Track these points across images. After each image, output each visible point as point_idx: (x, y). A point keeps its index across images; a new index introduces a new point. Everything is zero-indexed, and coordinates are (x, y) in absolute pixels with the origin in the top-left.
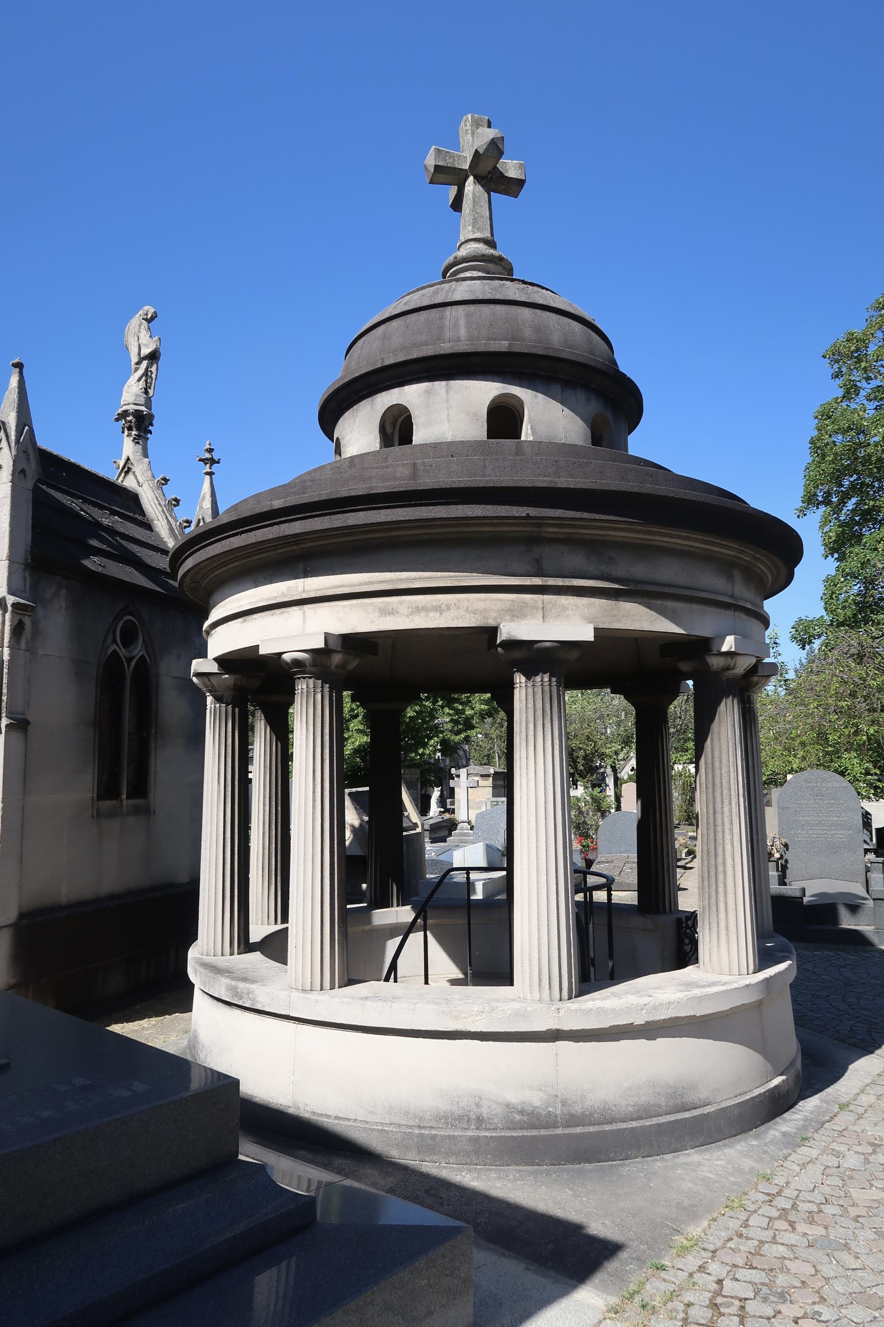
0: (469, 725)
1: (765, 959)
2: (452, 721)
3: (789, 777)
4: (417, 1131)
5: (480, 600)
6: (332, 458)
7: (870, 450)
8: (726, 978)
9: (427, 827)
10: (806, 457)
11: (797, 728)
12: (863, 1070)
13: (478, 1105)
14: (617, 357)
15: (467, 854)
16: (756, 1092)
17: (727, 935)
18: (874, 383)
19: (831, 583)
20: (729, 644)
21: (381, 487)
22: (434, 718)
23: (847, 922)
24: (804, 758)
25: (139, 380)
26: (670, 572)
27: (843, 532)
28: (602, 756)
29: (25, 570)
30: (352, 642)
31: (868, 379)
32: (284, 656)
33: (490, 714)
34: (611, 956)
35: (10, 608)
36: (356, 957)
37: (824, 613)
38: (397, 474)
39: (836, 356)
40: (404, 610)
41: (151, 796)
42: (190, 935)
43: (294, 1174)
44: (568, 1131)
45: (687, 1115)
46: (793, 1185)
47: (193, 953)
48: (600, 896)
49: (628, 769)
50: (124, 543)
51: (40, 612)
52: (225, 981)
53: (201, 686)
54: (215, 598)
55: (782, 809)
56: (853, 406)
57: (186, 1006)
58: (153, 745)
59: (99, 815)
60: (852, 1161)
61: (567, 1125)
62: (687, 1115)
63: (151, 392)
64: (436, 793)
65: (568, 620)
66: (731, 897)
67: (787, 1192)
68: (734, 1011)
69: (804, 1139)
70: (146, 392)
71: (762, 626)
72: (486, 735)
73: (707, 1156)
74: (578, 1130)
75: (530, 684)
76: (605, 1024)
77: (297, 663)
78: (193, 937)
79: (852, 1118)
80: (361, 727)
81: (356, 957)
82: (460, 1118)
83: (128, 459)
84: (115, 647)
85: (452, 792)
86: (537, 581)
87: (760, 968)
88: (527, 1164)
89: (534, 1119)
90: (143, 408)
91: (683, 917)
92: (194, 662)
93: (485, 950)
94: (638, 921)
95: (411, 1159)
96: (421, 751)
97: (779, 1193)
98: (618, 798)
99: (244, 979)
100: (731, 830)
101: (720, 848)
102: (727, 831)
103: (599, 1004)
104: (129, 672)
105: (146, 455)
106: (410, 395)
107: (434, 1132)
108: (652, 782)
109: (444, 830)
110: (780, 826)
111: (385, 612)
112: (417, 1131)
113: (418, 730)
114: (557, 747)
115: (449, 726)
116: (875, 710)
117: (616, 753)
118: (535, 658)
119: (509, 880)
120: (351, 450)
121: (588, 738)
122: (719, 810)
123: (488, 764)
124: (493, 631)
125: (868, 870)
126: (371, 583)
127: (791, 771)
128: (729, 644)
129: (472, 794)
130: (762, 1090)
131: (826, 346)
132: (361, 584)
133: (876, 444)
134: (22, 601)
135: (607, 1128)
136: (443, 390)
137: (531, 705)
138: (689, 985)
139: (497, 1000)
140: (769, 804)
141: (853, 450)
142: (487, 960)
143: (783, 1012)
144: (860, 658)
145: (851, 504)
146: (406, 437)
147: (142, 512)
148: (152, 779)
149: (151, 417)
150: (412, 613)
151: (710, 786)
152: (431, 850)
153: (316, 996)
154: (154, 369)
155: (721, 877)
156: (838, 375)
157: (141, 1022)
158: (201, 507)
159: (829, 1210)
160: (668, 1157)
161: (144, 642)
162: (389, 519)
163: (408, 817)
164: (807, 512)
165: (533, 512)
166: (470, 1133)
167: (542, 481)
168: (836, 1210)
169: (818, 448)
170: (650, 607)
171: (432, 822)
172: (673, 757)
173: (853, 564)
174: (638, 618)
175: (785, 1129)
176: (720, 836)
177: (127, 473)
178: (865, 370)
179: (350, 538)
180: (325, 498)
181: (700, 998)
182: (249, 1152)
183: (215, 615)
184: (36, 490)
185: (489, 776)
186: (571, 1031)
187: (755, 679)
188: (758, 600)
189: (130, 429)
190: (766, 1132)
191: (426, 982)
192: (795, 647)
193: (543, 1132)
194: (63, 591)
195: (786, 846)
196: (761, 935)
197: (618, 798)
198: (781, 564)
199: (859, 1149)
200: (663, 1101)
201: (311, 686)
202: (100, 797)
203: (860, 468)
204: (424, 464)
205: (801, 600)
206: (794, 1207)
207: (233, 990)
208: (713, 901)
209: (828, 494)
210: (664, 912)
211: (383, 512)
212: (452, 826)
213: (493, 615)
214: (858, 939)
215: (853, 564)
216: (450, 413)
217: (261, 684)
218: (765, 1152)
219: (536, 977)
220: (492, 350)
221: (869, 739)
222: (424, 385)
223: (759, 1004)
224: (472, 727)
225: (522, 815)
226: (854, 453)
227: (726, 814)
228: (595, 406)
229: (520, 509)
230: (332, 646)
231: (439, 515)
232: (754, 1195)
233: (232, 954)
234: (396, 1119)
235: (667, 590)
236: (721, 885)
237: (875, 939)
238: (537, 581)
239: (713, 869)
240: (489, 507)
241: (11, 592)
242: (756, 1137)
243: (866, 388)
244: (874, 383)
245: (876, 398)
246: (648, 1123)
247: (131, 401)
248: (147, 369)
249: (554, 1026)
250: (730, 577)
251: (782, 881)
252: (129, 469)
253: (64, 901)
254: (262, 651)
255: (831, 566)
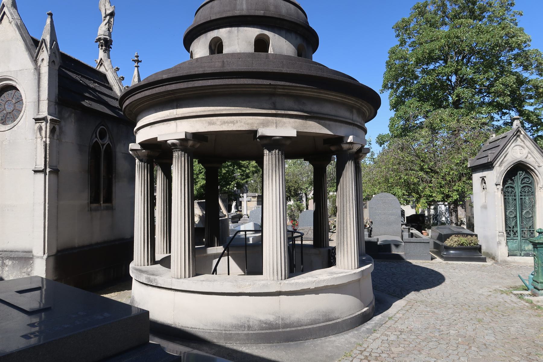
0: (248, 176)
1: (361, 263)
2: (241, 175)
3: (374, 196)
4: (224, 332)
5: (250, 119)
6: (189, 59)
7: (409, 67)
8: (346, 271)
9: (230, 217)
10: (384, 69)
11: (377, 177)
12: (398, 305)
13: (248, 321)
14: (309, 20)
15: (247, 226)
16: (357, 314)
17: (347, 254)
18: (412, 40)
19: (392, 120)
20: (350, 139)
21: (209, 70)
22: (233, 173)
23: (395, 251)
24: (379, 189)
25: (106, 25)
26: (327, 109)
27: (398, 100)
28: (301, 189)
29: (55, 105)
30: (197, 136)
31: (410, 38)
32: (168, 142)
33: (256, 172)
34: (302, 264)
35: (49, 121)
36: (199, 265)
37: (389, 132)
38: (216, 66)
39: (397, 28)
40: (218, 123)
41: (114, 202)
42: (131, 258)
43: (173, 348)
44: (284, 330)
45: (330, 323)
46: (370, 347)
47: (132, 265)
48: (298, 242)
49: (311, 195)
50: (100, 95)
51: (63, 123)
52: (145, 275)
53: (133, 155)
54: (139, 117)
55: (371, 208)
56: (403, 49)
57: (130, 288)
58: (114, 181)
59: (91, 210)
60: (392, 338)
61: (283, 328)
62: (330, 323)
63: (111, 30)
64: (234, 204)
65: (286, 128)
66: (349, 239)
67: (368, 350)
68: (349, 283)
69: (374, 330)
70: (109, 30)
71: (364, 133)
72: (255, 181)
73: (338, 338)
74: (288, 329)
75: (270, 154)
76: (299, 288)
77: (173, 144)
78: (132, 259)
79: (393, 322)
80: (204, 177)
81: (199, 265)
82: (241, 326)
83: (101, 59)
84: (97, 139)
85: (241, 205)
86: (274, 112)
87: (359, 267)
88: (268, 343)
89: (271, 326)
90: (108, 37)
91: (331, 249)
92: (130, 144)
93: (250, 259)
94: (314, 251)
95: (222, 343)
96: (228, 187)
97: (365, 350)
98: (307, 206)
99: (153, 275)
100: (350, 213)
101: (345, 220)
102: (348, 214)
103: (296, 281)
104: (103, 150)
105: (109, 58)
106: (222, 33)
107: (231, 332)
108: (320, 198)
109: (237, 218)
110: (370, 216)
111: (210, 123)
112: (224, 332)
113: (227, 178)
114: (281, 180)
115: (240, 177)
116: (407, 170)
117: (307, 188)
118: (272, 143)
119: (262, 236)
120: (197, 56)
121: (296, 182)
122: (345, 205)
123: (256, 192)
124: (256, 132)
125: (402, 231)
126: (205, 111)
127: (375, 194)
128: (350, 139)
129: (248, 204)
130: (359, 313)
131: (393, 24)
132: (200, 112)
133: (412, 65)
134: (55, 118)
135: (299, 328)
136: (236, 32)
137: (270, 163)
138: (332, 273)
139: (256, 280)
140: (366, 207)
141: (403, 67)
142: (252, 264)
143: (368, 283)
144: (402, 149)
145: (401, 89)
146: (220, 50)
147: (108, 83)
148: (114, 195)
149: (111, 41)
150: (222, 124)
151: (342, 196)
152: (231, 226)
153: (183, 280)
154: (112, 20)
155: (345, 231)
156: (398, 36)
157: (111, 294)
158: (134, 81)
159: (383, 355)
160: (323, 338)
161: (109, 137)
162: (212, 84)
163: (222, 212)
164: (384, 91)
165: (273, 82)
166: (245, 332)
167: (276, 69)
168: (386, 355)
169: (389, 65)
170: (319, 123)
171: (232, 215)
172: (329, 189)
173: (401, 113)
174: (315, 128)
175: (368, 327)
176: (345, 215)
177: (101, 65)
178: (409, 34)
179: (196, 92)
180: (185, 74)
181: (336, 278)
182: (154, 341)
183: (139, 125)
184: (59, 70)
185: (255, 197)
186: (286, 292)
187: (361, 154)
188: (363, 122)
189: (102, 46)
190: (360, 328)
191: (229, 274)
192: (378, 145)
193: (274, 331)
194: (73, 114)
195: (372, 222)
196: (360, 255)
197: (307, 206)
198: (372, 108)
199: (395, 333)
200: (321, 318)
201: (180, 154)
202: (91, 203)
203: (405, 74)
204: (227, 61)
205: (379, 125)
206: (370, 355)
207: (148, 279)
208: (342, 241)
209: (392, 85)
210: (324, 247)
211: (210, 81)
212: (241, 216)
213: (256, 125)
214: (398, 257)
215: (401, 113)
216: (239, 41)
217: (158, 155)
218: (360, 336)
219: (272, 271)
220: (257, 14)
221: (405, 181)
222: (228, 29)
223: (359, 280)
224: (249, 177)
225: (267, 210)
226: (403, 68)
227: (348, 207)
228: (299, 41)
229: (267, 81)
230: (188, 137)
231: (233, 83)
232: (355, 351)
233: (148, 265)
234: (216, 328)
235: (326, 116)
236: (345, 235)
237: (404, 257)
238: (274, 112)
239: (342, 229)
240: (254, 80)
241: (49, 114)
242: (356, 330)
243: (409, 42)
244: (412, 40)
245: (412, 46)
246: (315, 326)
247: (102, 34)
248: (109, 20)
249: (279, 290)
250: (352, 112)
251: (370, 236)
252: (102, 64)
253: (76, 245)
254: (159, 140)
255: (392, 113)
